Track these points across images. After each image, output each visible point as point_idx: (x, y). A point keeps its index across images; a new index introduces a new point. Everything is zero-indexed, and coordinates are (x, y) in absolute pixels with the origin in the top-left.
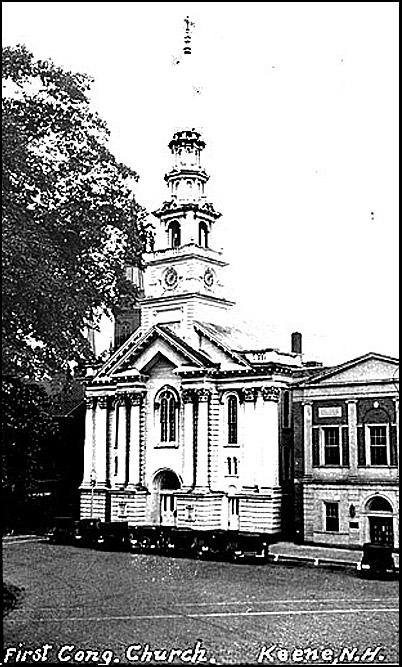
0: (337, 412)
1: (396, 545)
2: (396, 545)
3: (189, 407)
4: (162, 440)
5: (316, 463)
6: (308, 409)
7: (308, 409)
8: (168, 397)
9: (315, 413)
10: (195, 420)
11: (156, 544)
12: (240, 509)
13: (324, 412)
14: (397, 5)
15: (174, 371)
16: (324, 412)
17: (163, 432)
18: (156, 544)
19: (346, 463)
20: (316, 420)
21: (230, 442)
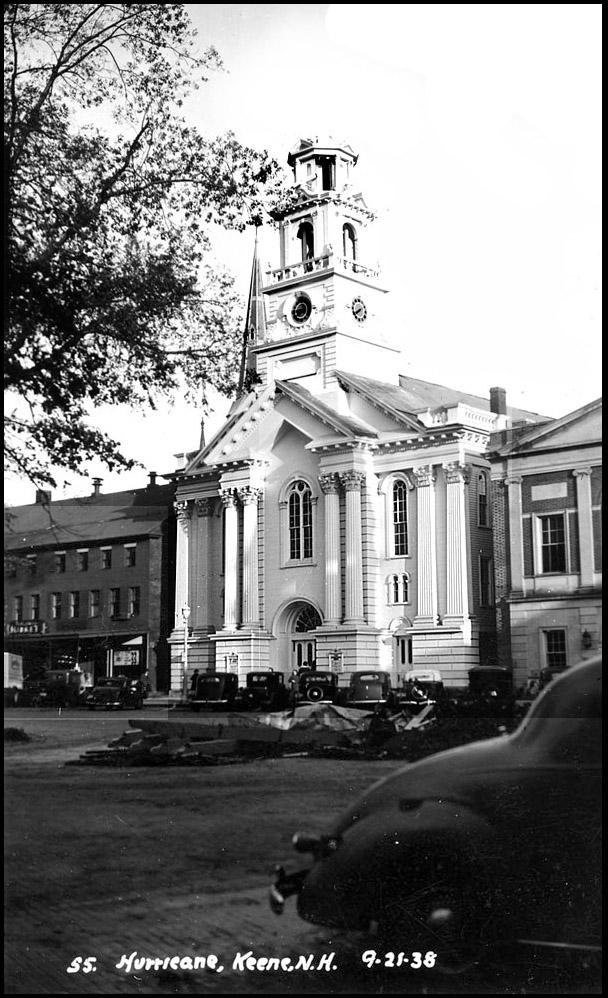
0: (560, 490)
1: (127, 963)
2: (127, 963)
3: (332, 500)
4: (292, 557)
5: (530, 572)
6: (515, 493)
7: (515, 493)
8: (301, 488)
9: (526, 495)
10: (342, 513)
11: (134, 686)
12: (414, 652)
13: (540, 493)
14: (599, 7)
15: (308, 446)
16: (540, 493)
17: (294, 545)
18: (134, 686)
19: (577, 569)
20: (529, 506)
21: (397, 553)
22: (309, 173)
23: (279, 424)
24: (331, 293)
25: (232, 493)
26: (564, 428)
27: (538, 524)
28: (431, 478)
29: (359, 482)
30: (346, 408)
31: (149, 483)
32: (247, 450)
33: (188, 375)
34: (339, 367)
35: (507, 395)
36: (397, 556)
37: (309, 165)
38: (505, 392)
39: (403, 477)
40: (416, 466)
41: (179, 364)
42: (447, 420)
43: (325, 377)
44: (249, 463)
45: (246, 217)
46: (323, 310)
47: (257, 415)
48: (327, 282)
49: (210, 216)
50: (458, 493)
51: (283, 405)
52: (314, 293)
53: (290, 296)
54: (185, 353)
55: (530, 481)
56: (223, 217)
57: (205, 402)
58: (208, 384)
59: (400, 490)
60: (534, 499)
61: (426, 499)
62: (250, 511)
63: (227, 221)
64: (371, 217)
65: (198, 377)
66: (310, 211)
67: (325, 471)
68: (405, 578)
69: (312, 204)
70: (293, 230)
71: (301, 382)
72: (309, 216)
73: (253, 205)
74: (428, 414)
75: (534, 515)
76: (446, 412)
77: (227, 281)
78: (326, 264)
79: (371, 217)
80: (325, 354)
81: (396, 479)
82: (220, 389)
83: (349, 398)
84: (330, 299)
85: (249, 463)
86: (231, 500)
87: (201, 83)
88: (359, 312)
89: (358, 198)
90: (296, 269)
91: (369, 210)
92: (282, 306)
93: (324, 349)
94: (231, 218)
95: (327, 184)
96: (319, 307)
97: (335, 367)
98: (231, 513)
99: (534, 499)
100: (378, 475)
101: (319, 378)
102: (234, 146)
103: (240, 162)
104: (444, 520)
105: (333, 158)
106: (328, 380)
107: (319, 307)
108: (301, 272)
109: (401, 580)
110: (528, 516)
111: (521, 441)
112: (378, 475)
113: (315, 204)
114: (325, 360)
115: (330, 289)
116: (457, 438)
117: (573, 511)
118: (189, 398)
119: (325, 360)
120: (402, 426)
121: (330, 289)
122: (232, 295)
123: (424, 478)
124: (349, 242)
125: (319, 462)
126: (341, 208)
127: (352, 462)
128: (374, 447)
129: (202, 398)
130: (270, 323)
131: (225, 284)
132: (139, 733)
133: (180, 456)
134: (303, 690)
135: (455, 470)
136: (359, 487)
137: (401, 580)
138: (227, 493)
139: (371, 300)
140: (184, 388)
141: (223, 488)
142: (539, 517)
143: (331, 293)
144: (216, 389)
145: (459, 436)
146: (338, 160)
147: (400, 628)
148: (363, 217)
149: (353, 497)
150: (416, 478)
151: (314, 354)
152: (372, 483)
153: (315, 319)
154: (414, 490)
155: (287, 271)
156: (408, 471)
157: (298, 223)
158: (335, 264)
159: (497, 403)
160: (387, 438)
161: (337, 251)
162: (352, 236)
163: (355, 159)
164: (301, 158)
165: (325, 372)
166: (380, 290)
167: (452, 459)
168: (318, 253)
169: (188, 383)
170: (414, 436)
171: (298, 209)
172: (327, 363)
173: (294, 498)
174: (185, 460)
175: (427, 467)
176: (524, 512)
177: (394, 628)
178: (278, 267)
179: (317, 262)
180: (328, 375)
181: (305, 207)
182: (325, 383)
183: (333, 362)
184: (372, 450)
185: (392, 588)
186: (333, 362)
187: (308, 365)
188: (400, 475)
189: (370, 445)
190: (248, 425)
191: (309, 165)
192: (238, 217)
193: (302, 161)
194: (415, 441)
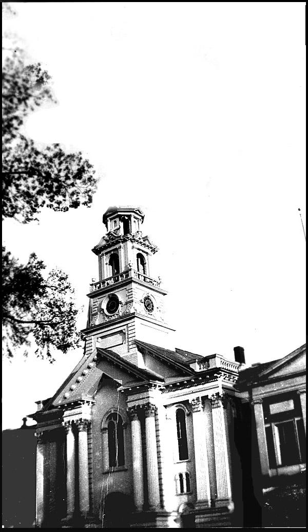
0: (291, 405)
6: (259, 411)
9: (266, 411)
13: (275, 408)
16: (275, 408)
20: (270, 418)
22: (115, 226)
23: (101, 375)
24: (131, 293)
25: (71, 423)
26: (288, 363)
27: (276, 430)
28: (201, 405)
29: (153, 411)
30: (142, 363)
31: (23, 424)
32: (80, 395)
33: (38, 338)
34: (137, 338)
35: (245, 352)
36: (181, 461)
37: (115, 222)
38: (244, 350)
39: (183, 407)
40: (190, 398)
41: (64, 393)
42: (209, 367)
43: (129, 345)
44: (82, 403)
45: (67, 204)
46: (126, 303)
47: (86, 371)
48: (128, 287)
49: (44, 202)
50: (219, 414)
51: (102, 364)
52: (121, 296)
53: (104, 299)
54: (37, 323)
55: (267, 402)
56: (53, 203)
57: (49, 354)
58: (50, 344)
59: (181, 417)
60: (272, 413)
61: (199, 420)
62: (83, 436)
63: (55, 205)
64: (154, 251)
65: (44, 340)
66: (117, 246)
67: (130, 405)
68: (187, 474)
69: (118, 242)
70: (106, 259)
71: (114, 350)
72: (116, 249)
73: (73, 194)
74: (196, 363)
75: (273, 424)
76: (208, 361)
77: (64, 276)
78: (127, 276)
79: (154, 251)
80: (128, 331)
81: (177, 408)
82: (58, 348)
83: (144, 359)
84: (130, 297)
85: (82, 403)
86: (70, 429)
87: (35, 107)
88: (148, 304)
89: (146, 239)
90: (109, 281)
91: (152, 246)
92: (100, 304)
93: (128, 327)
94: (59, 203)
95: (127, 230)
96: (123, 302)
97: (134, 338)
98: (70, 437)
99: (272, 413)
100: (166, 407)
101: (125, 346)
102: (59, 155)
103: (63, 166)
104: (211, 429)
105: (129, 216)
106: (130, 347)
107: (123, 302)
108: (111, 282)
109: (184, 476)
110: (268, 425)
111: (259, 375)
112: (166, 407)
113: (120, 242)
114: (128, 334)
115: (130, 291)
116: (217, 377)
117: (299, 419)
118: (39, 353)
119: (128, 334)
120: (180, 373)
121: (130, 291)
122: (66, 285)
123: (196, 406)
124: (141, 267)
125: (127, 399)
126: (135, 244)
127: (149, 397)
128: (162, 388)
129: (46, 352)
130: (93, 315)
131: (62, 279)
132: (299, 474)
133: (38, 403)
134: (190, 494)
135: (217, 399)
136: (154, 415)
137: (184, 476)
138: (68, 424)
139: (157, 299)
140: (34, 346)
141: (65, 421)
142: (276, 425)
143: (131, 293)
144: (55, 347)
145: (218, 376)
146: (133, 219)
147: (185, 510)
148: (149, 251)
149: (150, 421)
150: (191, 406)
151: (121, 332)
152: (161, 412)
153: (121, 310)
154: (190, 415)
155: (104, 283)
156: (186, 403)
157: (109, 255)
158: (132, 275)
159: (239, 354)
160: (170, 381)
161: (134, 267)
162: (143, 263)
163: (143, 218)
164: (110, 217)
165: (128, 342)
166: (160, 293)
167: (214, 392)
168: (123, 269)
169: (37, 343)
170: (188, 378)
171: (109, 246)
172: (130, 336)
173: (111, 425)
174: (42, 405)
175: (198, 399)
176: (266, 422)
177: (181, 511)
178: (97, 280)
179: (122, 276)
180: (130, 343)
181: (114, 244)
182: (129, 349)
183: (133, 335)
184: (161, 390)
185: (179, 482)
186: (133, 335)
187: (118, 339)
188: (179, 406)
189: (159, 386)
190: (80, 378)
191: (115, 222)
192: (63, 202)
193: (111, 219)
194: (189, 381)
